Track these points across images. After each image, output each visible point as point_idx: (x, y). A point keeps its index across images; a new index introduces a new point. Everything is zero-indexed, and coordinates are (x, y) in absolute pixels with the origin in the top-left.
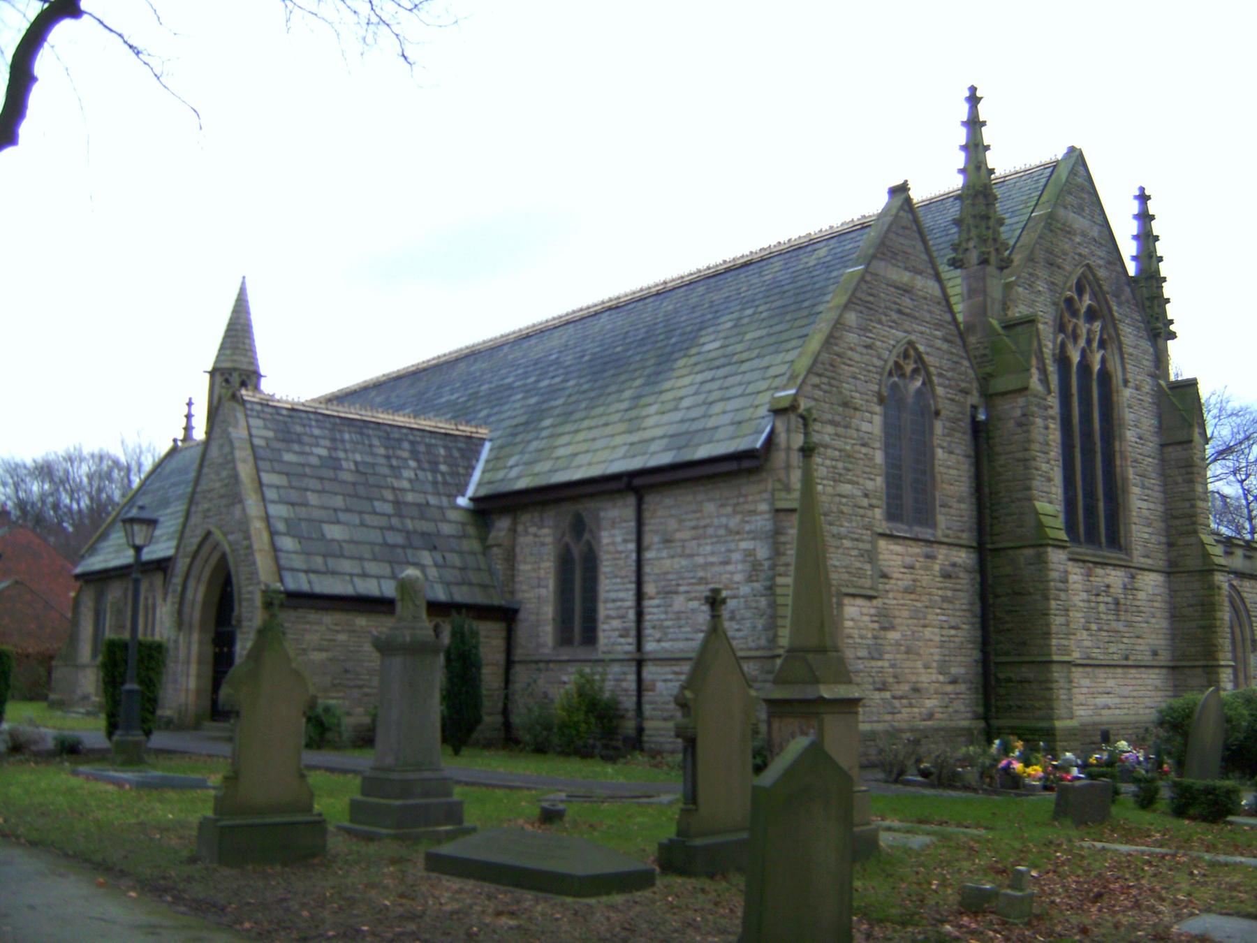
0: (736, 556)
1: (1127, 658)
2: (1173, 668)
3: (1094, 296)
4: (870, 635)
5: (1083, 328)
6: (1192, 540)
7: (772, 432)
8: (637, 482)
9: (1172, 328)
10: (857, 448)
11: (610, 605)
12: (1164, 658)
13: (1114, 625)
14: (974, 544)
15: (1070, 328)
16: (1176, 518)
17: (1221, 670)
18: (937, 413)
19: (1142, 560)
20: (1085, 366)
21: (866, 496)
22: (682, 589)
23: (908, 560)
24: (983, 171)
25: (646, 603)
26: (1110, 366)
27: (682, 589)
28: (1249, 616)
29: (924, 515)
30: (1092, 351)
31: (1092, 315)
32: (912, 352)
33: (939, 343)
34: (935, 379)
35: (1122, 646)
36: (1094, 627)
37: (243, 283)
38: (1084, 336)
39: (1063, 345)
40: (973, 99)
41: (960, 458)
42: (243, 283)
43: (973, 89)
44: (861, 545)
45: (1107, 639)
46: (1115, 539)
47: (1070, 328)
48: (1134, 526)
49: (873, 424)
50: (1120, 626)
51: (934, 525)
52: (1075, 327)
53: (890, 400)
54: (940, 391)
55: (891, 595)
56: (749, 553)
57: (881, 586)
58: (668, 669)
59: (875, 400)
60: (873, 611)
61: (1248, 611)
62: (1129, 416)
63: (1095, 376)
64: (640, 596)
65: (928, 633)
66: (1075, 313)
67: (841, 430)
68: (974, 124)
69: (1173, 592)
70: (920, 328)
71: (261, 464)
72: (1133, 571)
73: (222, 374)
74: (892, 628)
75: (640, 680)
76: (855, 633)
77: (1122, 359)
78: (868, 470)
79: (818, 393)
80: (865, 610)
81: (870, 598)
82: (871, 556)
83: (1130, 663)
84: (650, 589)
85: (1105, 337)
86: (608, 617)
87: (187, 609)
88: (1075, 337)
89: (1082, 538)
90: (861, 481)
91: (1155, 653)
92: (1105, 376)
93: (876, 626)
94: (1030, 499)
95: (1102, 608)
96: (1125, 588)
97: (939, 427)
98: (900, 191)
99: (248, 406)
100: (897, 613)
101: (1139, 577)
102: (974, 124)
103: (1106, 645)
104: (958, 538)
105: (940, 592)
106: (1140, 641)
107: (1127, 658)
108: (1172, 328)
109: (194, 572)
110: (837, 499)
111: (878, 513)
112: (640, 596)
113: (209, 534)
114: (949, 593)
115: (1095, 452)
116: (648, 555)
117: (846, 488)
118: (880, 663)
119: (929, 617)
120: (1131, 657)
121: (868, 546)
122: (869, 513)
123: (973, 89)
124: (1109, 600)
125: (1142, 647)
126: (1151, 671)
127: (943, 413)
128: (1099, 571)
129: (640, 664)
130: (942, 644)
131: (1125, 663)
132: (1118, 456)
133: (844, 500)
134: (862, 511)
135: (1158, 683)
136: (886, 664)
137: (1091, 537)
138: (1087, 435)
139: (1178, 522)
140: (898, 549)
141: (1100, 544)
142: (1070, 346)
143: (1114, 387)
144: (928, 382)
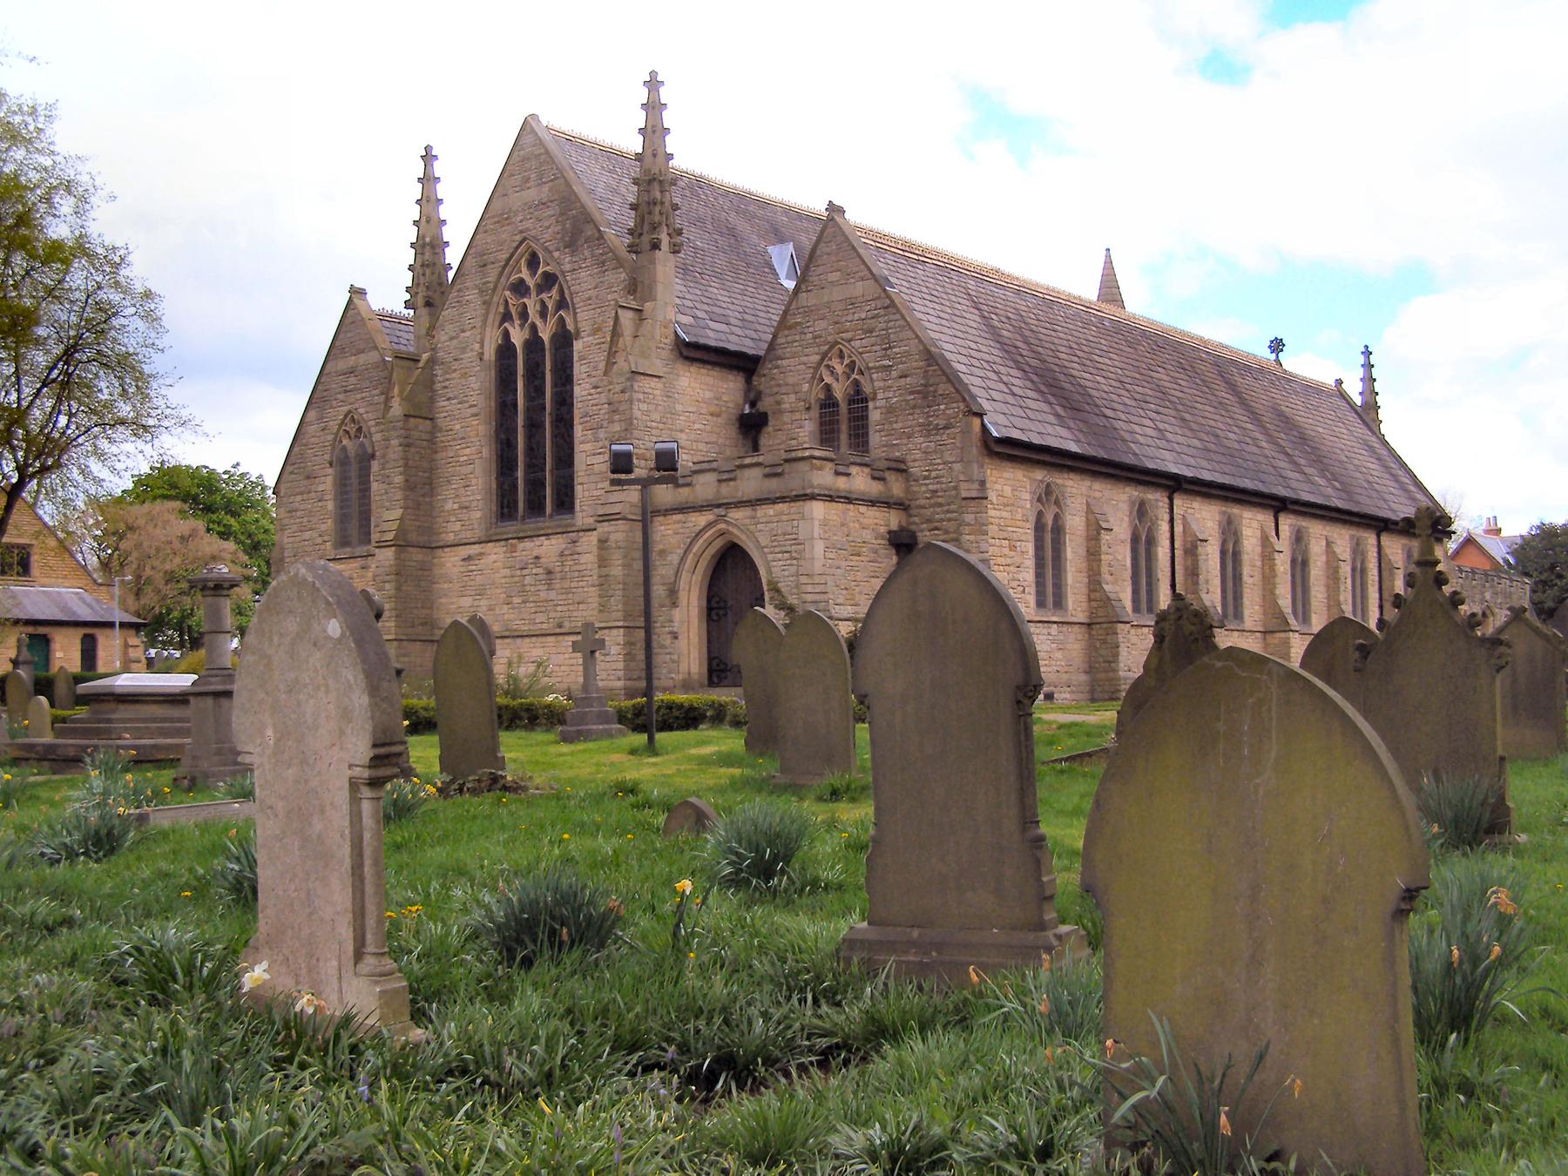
5: (532, 304)
9: (408, 297)
24: (660, 159)
36: (517, 600)
37: (1109, 264)
40: (428, 157)
42: (1109, 264)
43: (428, 149)
45: (533, 610)
68: (428, 180)
70: (359, 396)
92: (564, 339)
101: (584, 539)
102: (428, 180)
103: (533, 616)
107: (560, 627)
108: (408, 297)
117: (307, 535)
120: (567, 624)
122: (323, 547)
123: (428, 149)
124: (540, 570)
128: (521, 545)
131: (558, 631)
137: (536, 507)
138: (535, 408)
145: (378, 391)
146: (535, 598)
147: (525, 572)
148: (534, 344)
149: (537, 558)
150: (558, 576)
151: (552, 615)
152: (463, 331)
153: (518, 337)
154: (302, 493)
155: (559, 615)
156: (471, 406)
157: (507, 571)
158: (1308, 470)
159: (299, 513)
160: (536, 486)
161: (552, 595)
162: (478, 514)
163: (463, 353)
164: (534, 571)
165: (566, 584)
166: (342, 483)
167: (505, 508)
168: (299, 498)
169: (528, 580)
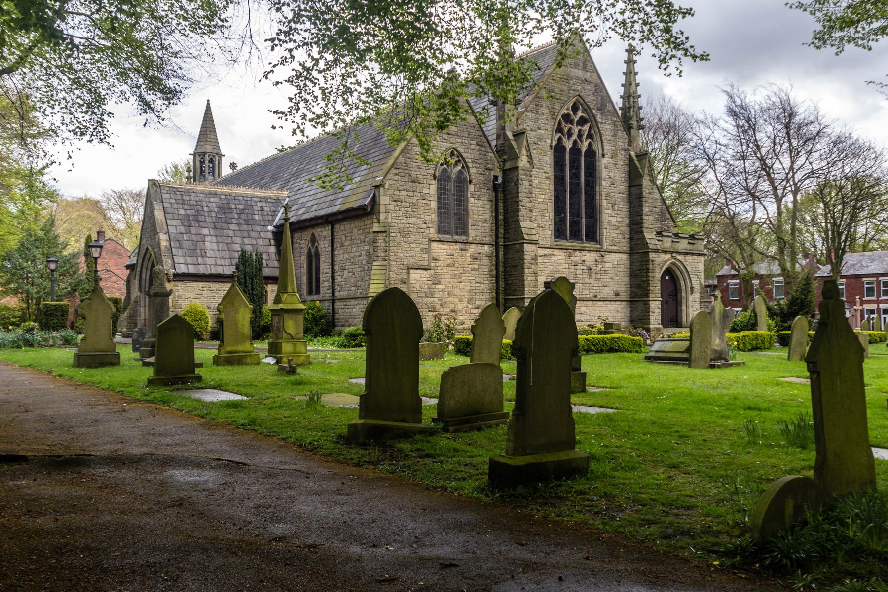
0: (363, 253)
1: (596, 297)
2: (631, 302)
3: (584, 111)
4: (426, 286)
6: (640, 236)
7: (374, 194)
8: (329, 219)
10: (421, 201)
11: (324, 275)
12: (623, 296)
13: (587, 280)
14: (494, 243)
15: (566, 130)
16: (634, 225)
17: (651, 303)
18: (470, 182)
19: (611, 247)
20: (575, 150)
21: (425, 223)
22: (347, 268)
23: (450, 252)
25: (336, 274)
26: (595, 147)
27: (347, 268)
28: (689, 275)
29: (462, 228)
30: (581, 141)
31: (582, 122)
32: (456, 153)
33: (473, 147)
34: (470, 165)
35: (592, 291)
37: (208, 104)
38: (577, 133)
39: (560, 139)
41: (486, 202)
42: (208, 104)
44: (421, 246)
46: (593, 235)
47: (566, 130)
48: (605, 230)
49: (432, 189)
50: (592, 281)
51: (467, 235)
52: (570, 129)
53: (442, 179)
54: (473, 170)
55: (439, 268)
56: (368, 251)
57: (432, 265)
58: (342, 304)
59: (432, 178)
60: (428, 276)
61: (688, 272)
62: (604, 173)
63: (583, 153)
64: (333, 272)
65: (461, 285)
66: (571, 122)
67: (410, 194)
69: (632, 263)
71: (168, 216)
72: (603, 253)
73: (200, 156)
74: (440, 283)
75: (333, 309)
76: (418, 286)
77: (602, 142)
78: (426, 211)
79: (396, 178)
80: (423, 276)
81: (426, 270)
82: (428, 251)
83: (597, 299)
84: (337, 268)
85: (592, 132)
86: (323, 281)
87: (143, 283)
88: (570, 134)
89: (568, 238)
90: (422, 216)
91: (617, 294)
92: (591, 153)
93: (430, 282)
94: (518, 221)
95: (579, 272)
96: (596, 261)
97: (471, 188)
98: (224, 156)
99: (162, 188)
100: (443, 276)
104: (475, 240)
105: (470, 266)
106: (606, 288)
109: (145, 266)
110: (408, 225)
111: (432, 231)
112: (333, 272)
113: (147, 249)
114: (476, 267)
115: (581, 193)
116: (336, 252)
117: (414, 220)
118: (432, 299)
119: (463, 278)
120: (599, 296)
121: (427, 246)
122: (427, 231)
124: (585, 268)
125: (608, 293)
126: (617, 303)
127: (473, 181)
128: (578, 253)
129: (333, 301)
130: (471, 291)
131: (594, 299)
132: (598, 194)
133: (411, 226)
134: (422, 230)
135: (620, 309)
136: (436, 300)
137: (575, 235)
138: (575, 186)
139: (635, 227)
140: (444, 247)
141: (582, 240)
142: (565, 140)
143: (597, 159)
144: (466, 167)
145: (474, 142)
146: (583, 282)
147: (576, 267)
148: (575, 150)
149: (584, 261)
150: (595, 272)
151: (592, 291)
152: (539, 129)
153: (568, 145)
154: (407, 191)
155: (594, 291)
156: (545, 173)
157: (567, 266)
158: (553, 559)
159: (403, 204)
160: (575, 224)
161: (592, 281)
162: (549, 233)
163: (540, 141)
164: (582, 268)
165: (599, 276)
166: (442, 193)
167: (559, 233)
168: (404, 193)
169: (579, 272)
